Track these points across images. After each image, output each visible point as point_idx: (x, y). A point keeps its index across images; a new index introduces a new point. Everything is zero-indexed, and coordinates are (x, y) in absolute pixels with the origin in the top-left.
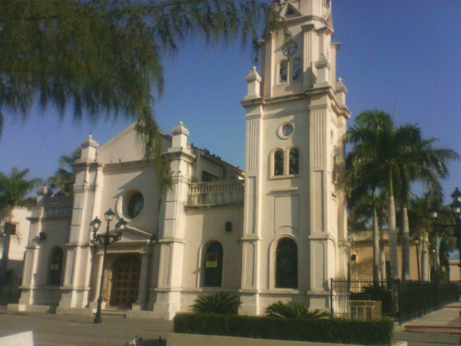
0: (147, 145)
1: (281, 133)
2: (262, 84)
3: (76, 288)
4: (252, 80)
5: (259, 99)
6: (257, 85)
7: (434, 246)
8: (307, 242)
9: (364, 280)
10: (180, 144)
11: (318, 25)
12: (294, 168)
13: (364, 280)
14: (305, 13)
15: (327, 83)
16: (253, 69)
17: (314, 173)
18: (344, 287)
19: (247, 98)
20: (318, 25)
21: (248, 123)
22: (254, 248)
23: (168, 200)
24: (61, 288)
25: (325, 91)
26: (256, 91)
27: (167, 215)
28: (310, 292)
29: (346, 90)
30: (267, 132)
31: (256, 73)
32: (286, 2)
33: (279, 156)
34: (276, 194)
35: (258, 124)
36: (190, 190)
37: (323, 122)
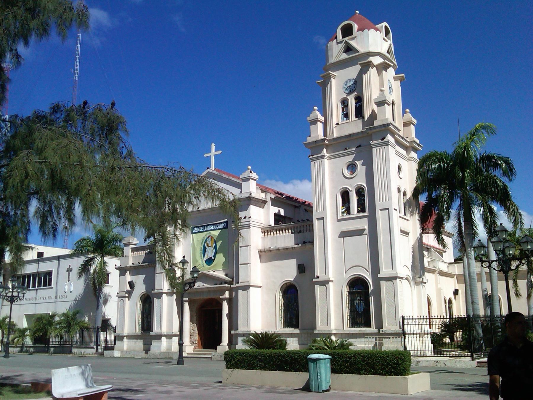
0: (17, 392)
1: (347, 173)
2: (325, 124)
3: (334, 328)
4: (315, 121)
5: (323, 140)
6: (320, 126)
7: (5, 348)
8: (377, 281)
9: (458, 316)
10: (249, 189)
11: (377, 60)
12: (361, 207)
13: (458, 316)
14: (362, 49)
15: (387, 119)
16: (314, 110)
17: (380, 211)
18: (427, 324)
19: (310, 140)
20: (377, 60)
21: (312, 163)
22: (327, 290)
23: (241, 245)
24: (151, 333)
25: (386, 129)
26: (318, 132)
27: (242, 260)
28: (382, 331)
29: (415, 121)
30: (332, 172)
31: (318, 113)
32: (343, 39)
33: (345, 195)
34: (344, 234)
35: (323, 165)
36: (263, 234)
37: (387, 160)
